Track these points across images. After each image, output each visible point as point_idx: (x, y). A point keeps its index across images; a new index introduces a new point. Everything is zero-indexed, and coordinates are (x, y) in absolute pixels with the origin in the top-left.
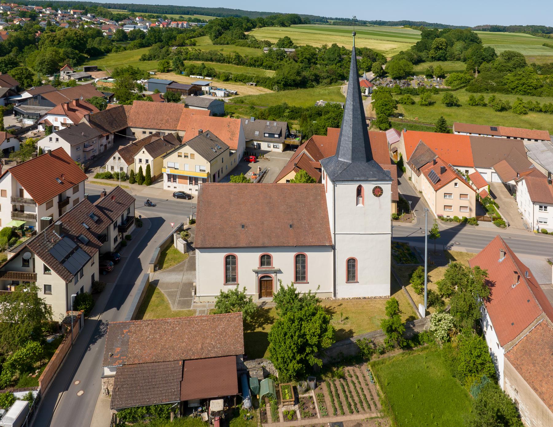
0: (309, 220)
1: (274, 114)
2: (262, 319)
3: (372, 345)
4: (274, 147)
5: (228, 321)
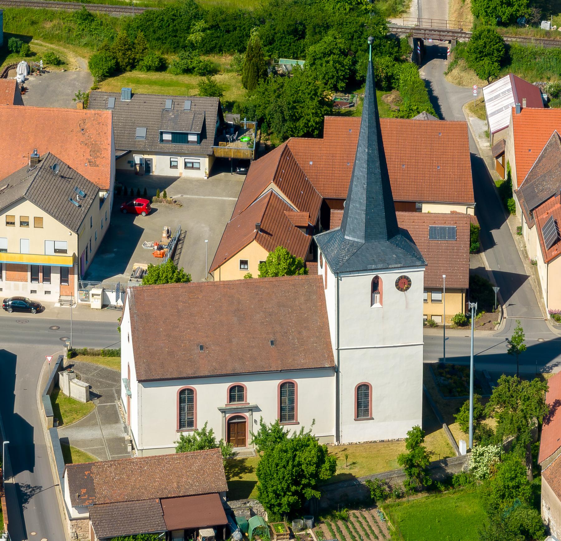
0: (300, 333)
1: (158, 39)
2: (237, 469)
3: (386, 487)
4: (186, 167)
5: (204, 458)
